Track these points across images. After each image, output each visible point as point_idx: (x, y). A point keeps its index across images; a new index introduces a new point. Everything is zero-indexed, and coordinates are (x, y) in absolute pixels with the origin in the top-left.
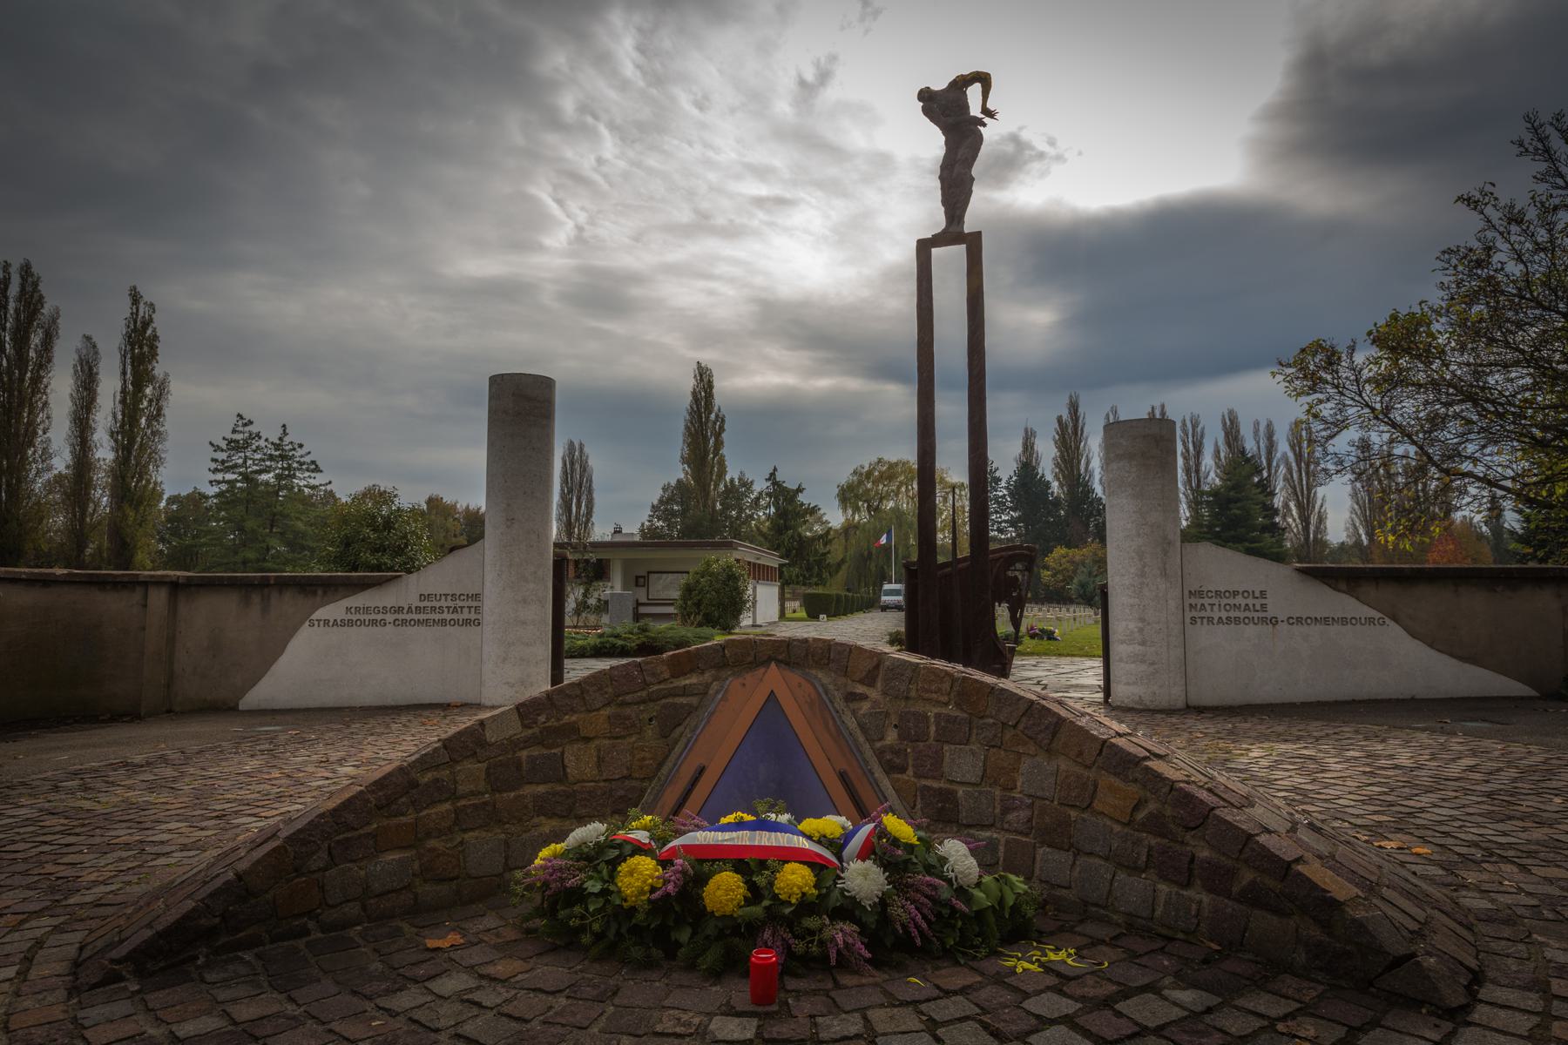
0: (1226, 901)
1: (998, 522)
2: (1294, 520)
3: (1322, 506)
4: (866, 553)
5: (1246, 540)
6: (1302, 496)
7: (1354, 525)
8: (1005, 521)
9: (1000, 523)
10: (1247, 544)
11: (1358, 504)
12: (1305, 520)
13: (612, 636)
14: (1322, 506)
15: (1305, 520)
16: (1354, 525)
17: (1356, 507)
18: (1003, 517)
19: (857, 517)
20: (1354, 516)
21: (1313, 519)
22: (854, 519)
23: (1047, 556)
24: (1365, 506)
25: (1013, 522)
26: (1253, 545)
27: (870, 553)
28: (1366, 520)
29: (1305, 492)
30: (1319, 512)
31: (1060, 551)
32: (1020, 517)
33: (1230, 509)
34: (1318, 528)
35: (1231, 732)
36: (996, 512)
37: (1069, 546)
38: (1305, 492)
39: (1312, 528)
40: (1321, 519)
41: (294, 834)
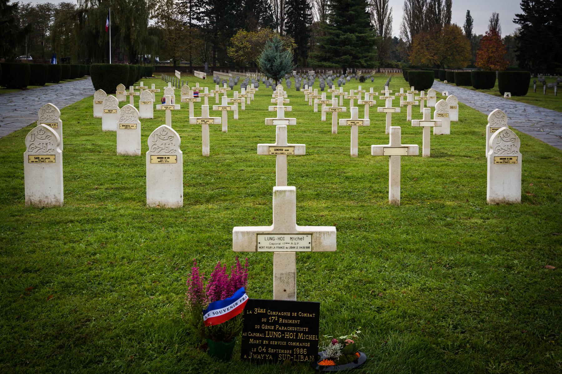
0: (60, 151)
1: (197, 13)
2: (375, 22)
3: (390, 13)
4: (94, 31)
5: (356, 32)
6: (380, 8)
7: (404, 26)
8: (202, 12)
9: (199, 13)
10: (357, 34)
11: (407, 14)
12: (381, 22)
13: (466, 100)
14: (390, 14)
15: (381, 22)
16: (404, 26)
17: (406, 16)
18: (201, 9)
19: (89, 5)
20: (405, 21)
21: (386, 21)
22: (87, 6)
23: (232, 37)
24: (410, 16)
25: (207, 13)
26: (361, 35)
27: (98, 32)
28: (411, 24)
29: (382, 5)
30: (389, 17)
31: (242, 33)
32: (213, 9)
33: (348, 11)
34: (387, 27)
35: (501, 100)
36: (196, 6)
37: (248, 30)
38: (382, 5)
39: (384, 26)
40: (389, 22)
41: (184, 177)
